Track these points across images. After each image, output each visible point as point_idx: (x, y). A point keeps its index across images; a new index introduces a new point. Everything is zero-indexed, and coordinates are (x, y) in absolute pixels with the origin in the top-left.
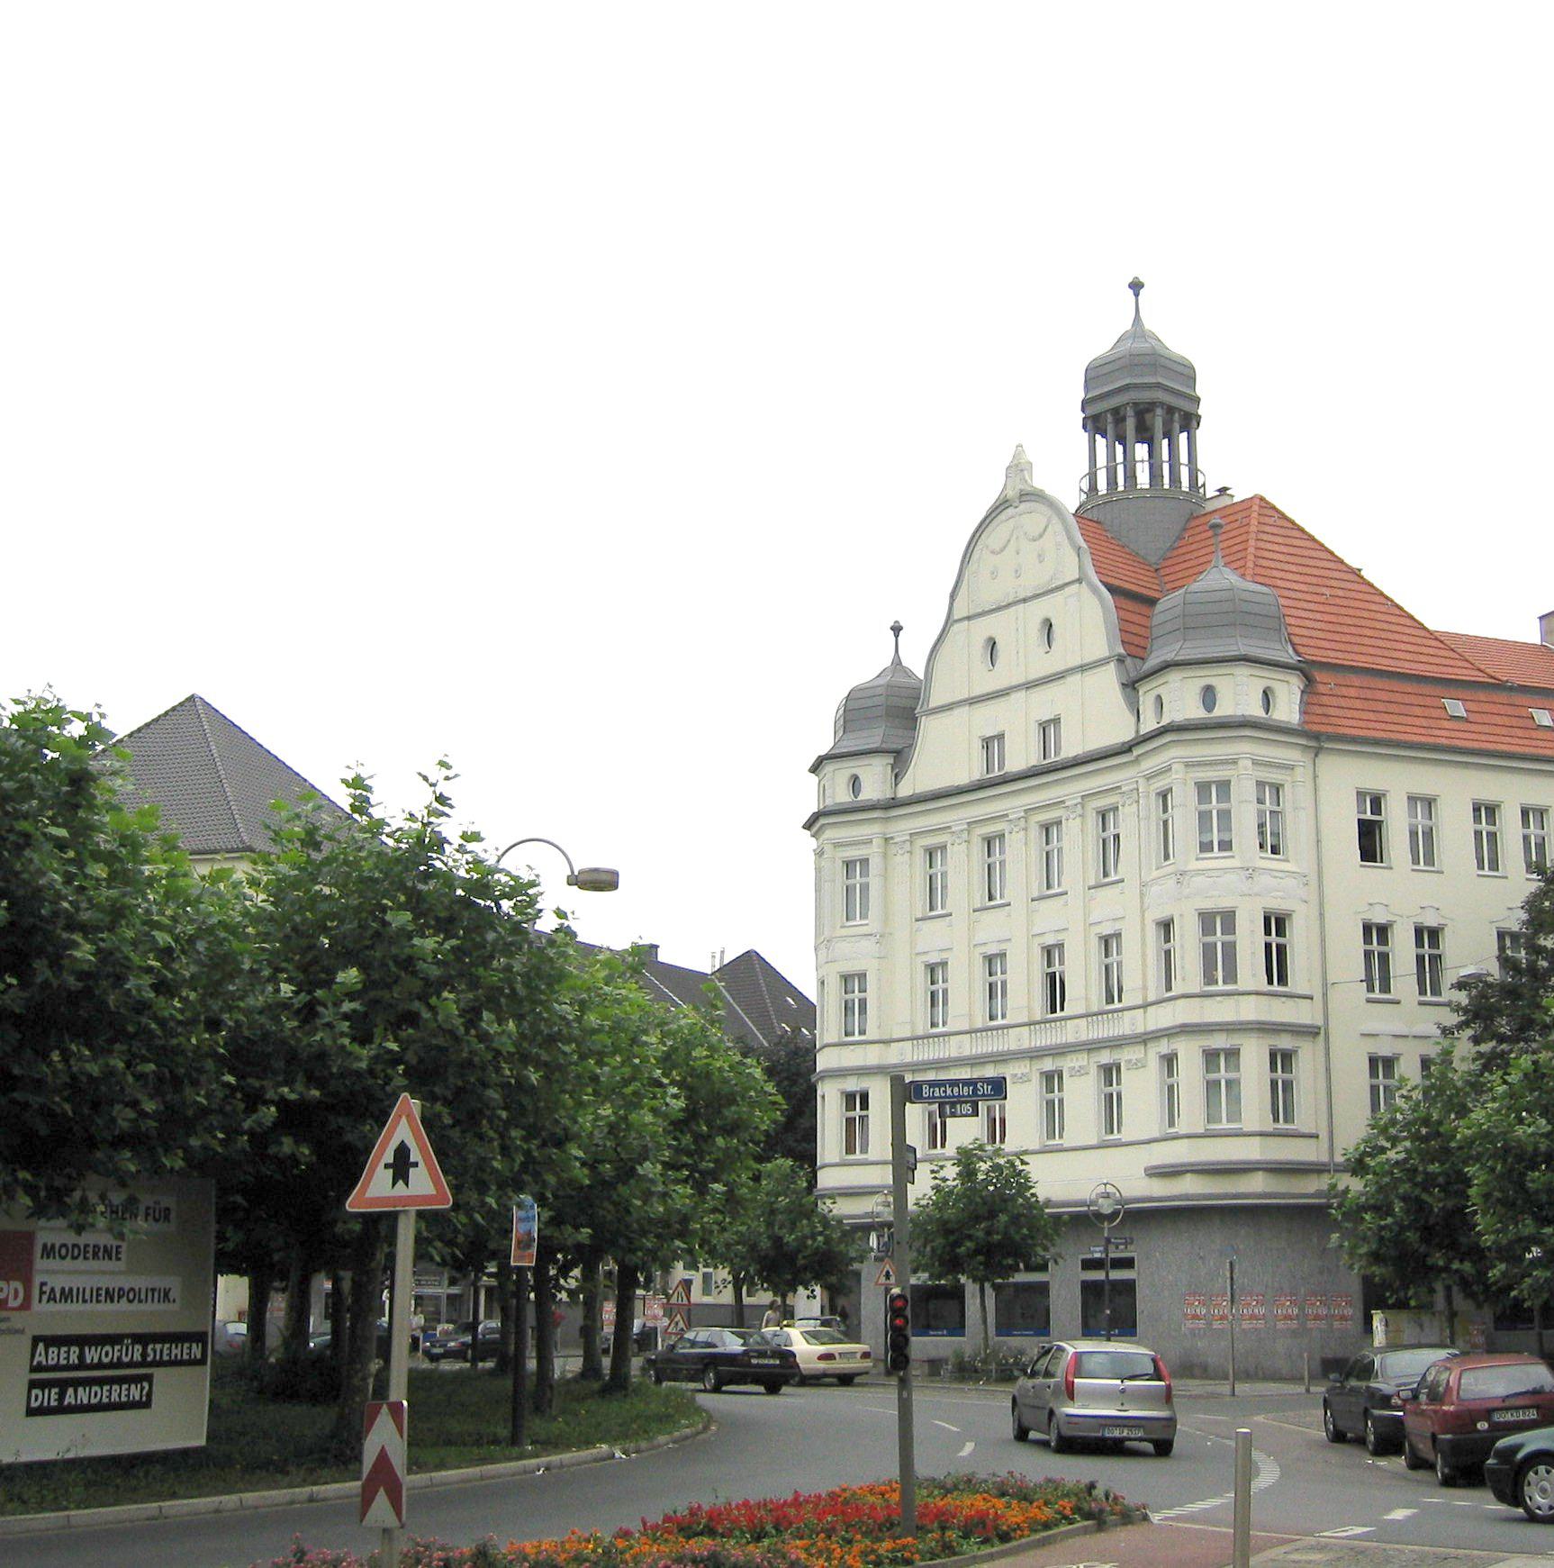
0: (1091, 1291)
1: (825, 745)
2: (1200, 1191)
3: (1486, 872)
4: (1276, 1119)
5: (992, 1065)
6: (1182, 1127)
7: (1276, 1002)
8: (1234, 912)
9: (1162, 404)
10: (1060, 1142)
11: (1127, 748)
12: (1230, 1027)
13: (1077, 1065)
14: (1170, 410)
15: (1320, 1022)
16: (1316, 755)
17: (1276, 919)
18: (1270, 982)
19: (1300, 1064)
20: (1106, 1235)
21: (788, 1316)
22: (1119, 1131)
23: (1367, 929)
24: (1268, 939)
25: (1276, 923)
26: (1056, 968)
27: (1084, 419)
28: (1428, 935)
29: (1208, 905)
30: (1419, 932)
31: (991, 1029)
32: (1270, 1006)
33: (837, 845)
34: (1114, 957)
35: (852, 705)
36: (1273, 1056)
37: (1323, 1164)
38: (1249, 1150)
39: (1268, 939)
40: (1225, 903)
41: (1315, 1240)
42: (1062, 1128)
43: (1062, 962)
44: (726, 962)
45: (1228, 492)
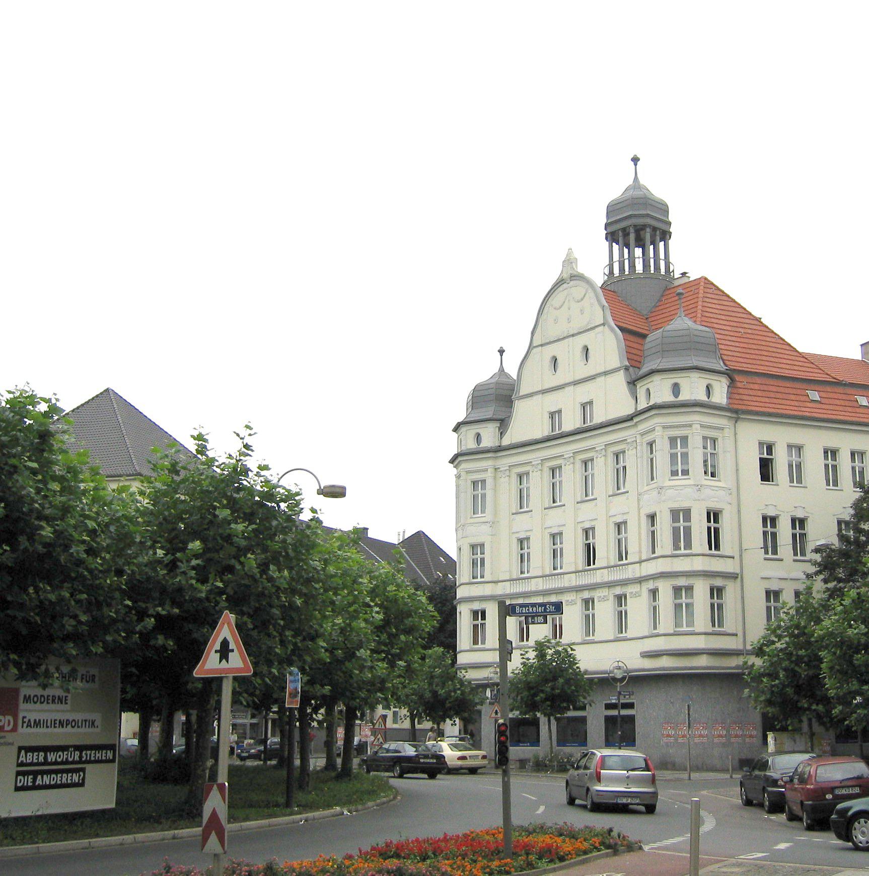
0: (610, 721)
1: (461, 416)
2: (671, 665)
3: (831, 487)
4: (714, 625)
5: (555, 595)
6: (661, 630)
7: (714, 560)
8: (690, 509)
9: (650, 226)
10: (593, 638)
11: (630, 418)
12: (688, 574)
13: (602, 595)
14: (654, 229)
15: (738, 571)
16: (736, 422)
17: (714, 514)
18: (710, 549)
19: (727, 595)
20: (618, 690)
21: (441, 735)
22: (626, 632)
23: (765, 519)
24: (709, 525)
25: (714, 516)
26: (591, 541)
27: (606, 234)
28: (799, 523)
29: (676, 505)
30: (793, 521)
31: (554, 575)
32: (710, 562)
33: (468, 472)
34: (623, 535)
35: (476, 394)
36: (712, 590)
37: (740, 650)
38: (699, 643)
39: (709, 525)
40: (685, 504)
41: (735, 693)
42: (594, 630)
43: (594, 538)
44: (406, 537)
45: (687, 275)
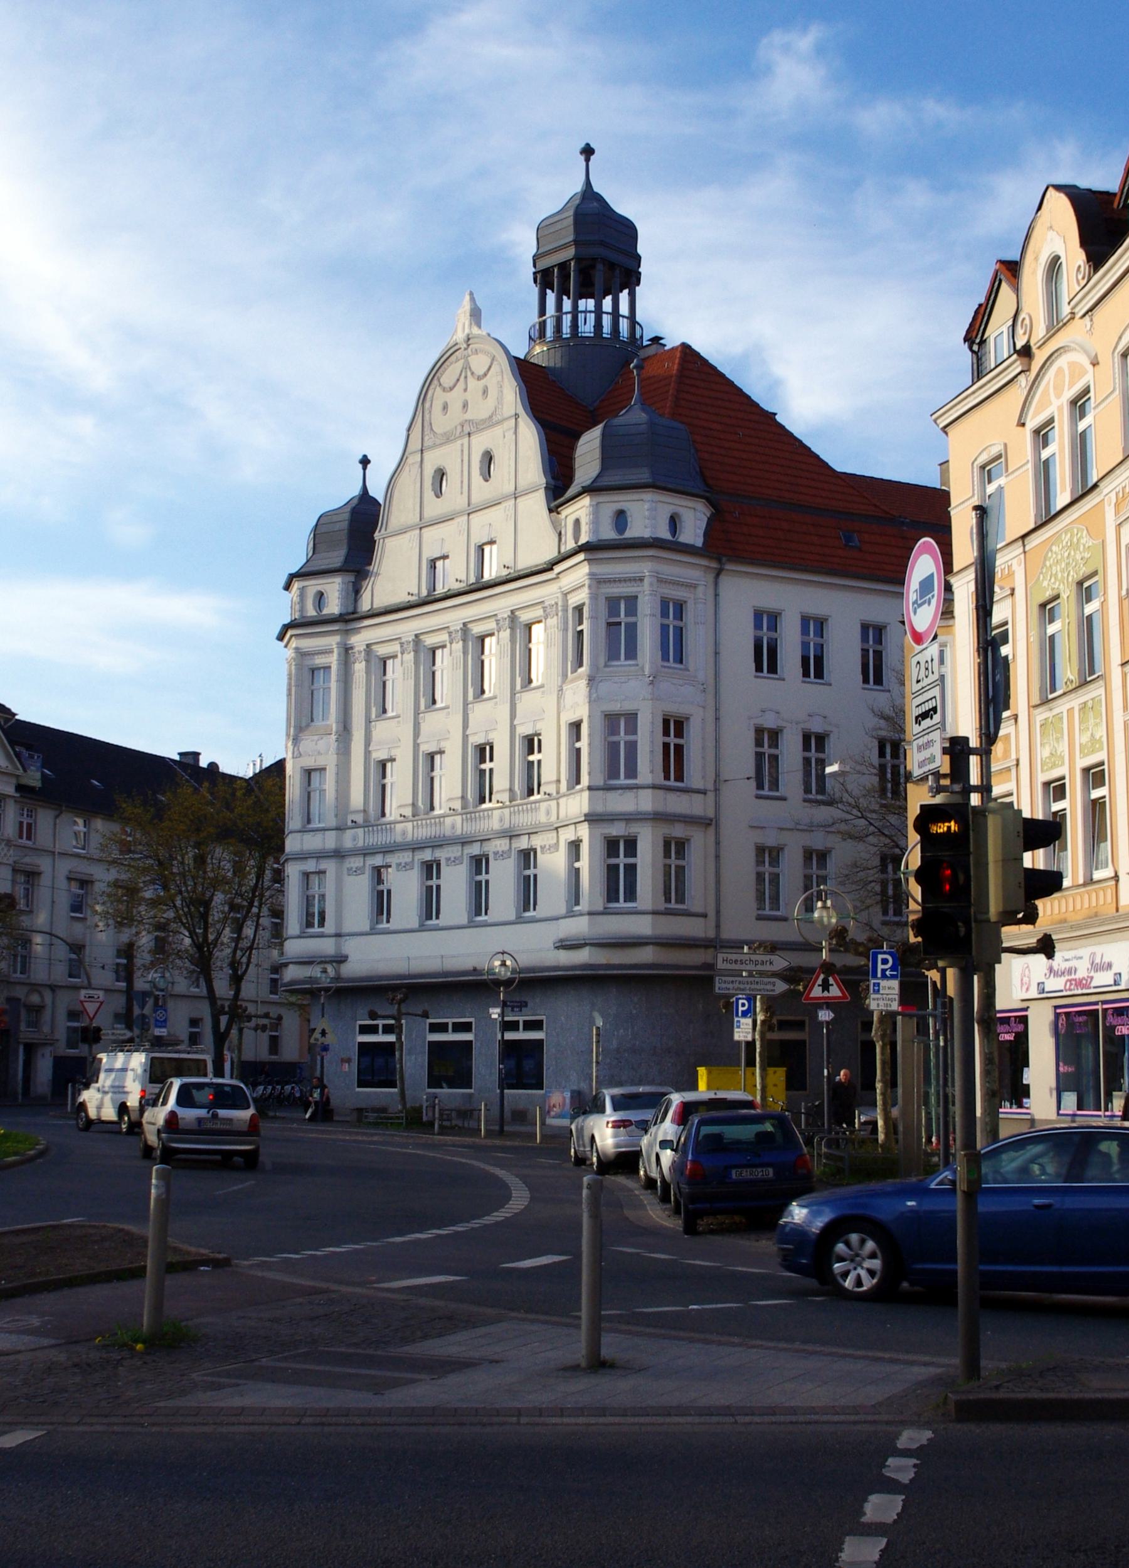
2: (604, 961)
3: (671, 663)
4: (668, 900)
9: (604, 261)
12: (687, 819)
13: (452, 855)
14: (611, 266)
16: (718, 575)
17: (675, 722)
18: (667, 777)
19: (692, 849)
21: (202, 1073)
22: (534, 909)
23: (759, 731)
24: (667, 740)
25: (673, 725)
27: (535, 273)
28: (814, 741)
29: (615, 707)
30: (806, 737)
32: (665, 799)
35: (321, 530)
36: (667, 844)
37: (711, 940)
38: (642, 926)
39: (667, 740)
40: (629, 706)
42: (535, 904)
45: (661, 341)
